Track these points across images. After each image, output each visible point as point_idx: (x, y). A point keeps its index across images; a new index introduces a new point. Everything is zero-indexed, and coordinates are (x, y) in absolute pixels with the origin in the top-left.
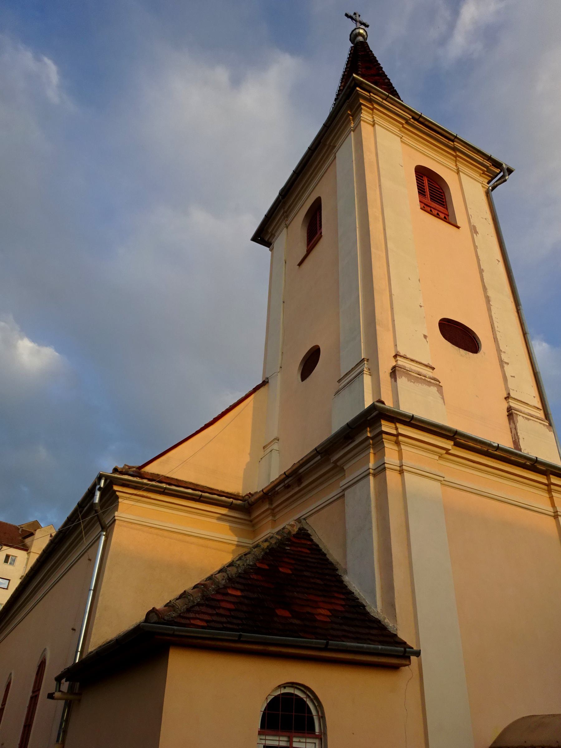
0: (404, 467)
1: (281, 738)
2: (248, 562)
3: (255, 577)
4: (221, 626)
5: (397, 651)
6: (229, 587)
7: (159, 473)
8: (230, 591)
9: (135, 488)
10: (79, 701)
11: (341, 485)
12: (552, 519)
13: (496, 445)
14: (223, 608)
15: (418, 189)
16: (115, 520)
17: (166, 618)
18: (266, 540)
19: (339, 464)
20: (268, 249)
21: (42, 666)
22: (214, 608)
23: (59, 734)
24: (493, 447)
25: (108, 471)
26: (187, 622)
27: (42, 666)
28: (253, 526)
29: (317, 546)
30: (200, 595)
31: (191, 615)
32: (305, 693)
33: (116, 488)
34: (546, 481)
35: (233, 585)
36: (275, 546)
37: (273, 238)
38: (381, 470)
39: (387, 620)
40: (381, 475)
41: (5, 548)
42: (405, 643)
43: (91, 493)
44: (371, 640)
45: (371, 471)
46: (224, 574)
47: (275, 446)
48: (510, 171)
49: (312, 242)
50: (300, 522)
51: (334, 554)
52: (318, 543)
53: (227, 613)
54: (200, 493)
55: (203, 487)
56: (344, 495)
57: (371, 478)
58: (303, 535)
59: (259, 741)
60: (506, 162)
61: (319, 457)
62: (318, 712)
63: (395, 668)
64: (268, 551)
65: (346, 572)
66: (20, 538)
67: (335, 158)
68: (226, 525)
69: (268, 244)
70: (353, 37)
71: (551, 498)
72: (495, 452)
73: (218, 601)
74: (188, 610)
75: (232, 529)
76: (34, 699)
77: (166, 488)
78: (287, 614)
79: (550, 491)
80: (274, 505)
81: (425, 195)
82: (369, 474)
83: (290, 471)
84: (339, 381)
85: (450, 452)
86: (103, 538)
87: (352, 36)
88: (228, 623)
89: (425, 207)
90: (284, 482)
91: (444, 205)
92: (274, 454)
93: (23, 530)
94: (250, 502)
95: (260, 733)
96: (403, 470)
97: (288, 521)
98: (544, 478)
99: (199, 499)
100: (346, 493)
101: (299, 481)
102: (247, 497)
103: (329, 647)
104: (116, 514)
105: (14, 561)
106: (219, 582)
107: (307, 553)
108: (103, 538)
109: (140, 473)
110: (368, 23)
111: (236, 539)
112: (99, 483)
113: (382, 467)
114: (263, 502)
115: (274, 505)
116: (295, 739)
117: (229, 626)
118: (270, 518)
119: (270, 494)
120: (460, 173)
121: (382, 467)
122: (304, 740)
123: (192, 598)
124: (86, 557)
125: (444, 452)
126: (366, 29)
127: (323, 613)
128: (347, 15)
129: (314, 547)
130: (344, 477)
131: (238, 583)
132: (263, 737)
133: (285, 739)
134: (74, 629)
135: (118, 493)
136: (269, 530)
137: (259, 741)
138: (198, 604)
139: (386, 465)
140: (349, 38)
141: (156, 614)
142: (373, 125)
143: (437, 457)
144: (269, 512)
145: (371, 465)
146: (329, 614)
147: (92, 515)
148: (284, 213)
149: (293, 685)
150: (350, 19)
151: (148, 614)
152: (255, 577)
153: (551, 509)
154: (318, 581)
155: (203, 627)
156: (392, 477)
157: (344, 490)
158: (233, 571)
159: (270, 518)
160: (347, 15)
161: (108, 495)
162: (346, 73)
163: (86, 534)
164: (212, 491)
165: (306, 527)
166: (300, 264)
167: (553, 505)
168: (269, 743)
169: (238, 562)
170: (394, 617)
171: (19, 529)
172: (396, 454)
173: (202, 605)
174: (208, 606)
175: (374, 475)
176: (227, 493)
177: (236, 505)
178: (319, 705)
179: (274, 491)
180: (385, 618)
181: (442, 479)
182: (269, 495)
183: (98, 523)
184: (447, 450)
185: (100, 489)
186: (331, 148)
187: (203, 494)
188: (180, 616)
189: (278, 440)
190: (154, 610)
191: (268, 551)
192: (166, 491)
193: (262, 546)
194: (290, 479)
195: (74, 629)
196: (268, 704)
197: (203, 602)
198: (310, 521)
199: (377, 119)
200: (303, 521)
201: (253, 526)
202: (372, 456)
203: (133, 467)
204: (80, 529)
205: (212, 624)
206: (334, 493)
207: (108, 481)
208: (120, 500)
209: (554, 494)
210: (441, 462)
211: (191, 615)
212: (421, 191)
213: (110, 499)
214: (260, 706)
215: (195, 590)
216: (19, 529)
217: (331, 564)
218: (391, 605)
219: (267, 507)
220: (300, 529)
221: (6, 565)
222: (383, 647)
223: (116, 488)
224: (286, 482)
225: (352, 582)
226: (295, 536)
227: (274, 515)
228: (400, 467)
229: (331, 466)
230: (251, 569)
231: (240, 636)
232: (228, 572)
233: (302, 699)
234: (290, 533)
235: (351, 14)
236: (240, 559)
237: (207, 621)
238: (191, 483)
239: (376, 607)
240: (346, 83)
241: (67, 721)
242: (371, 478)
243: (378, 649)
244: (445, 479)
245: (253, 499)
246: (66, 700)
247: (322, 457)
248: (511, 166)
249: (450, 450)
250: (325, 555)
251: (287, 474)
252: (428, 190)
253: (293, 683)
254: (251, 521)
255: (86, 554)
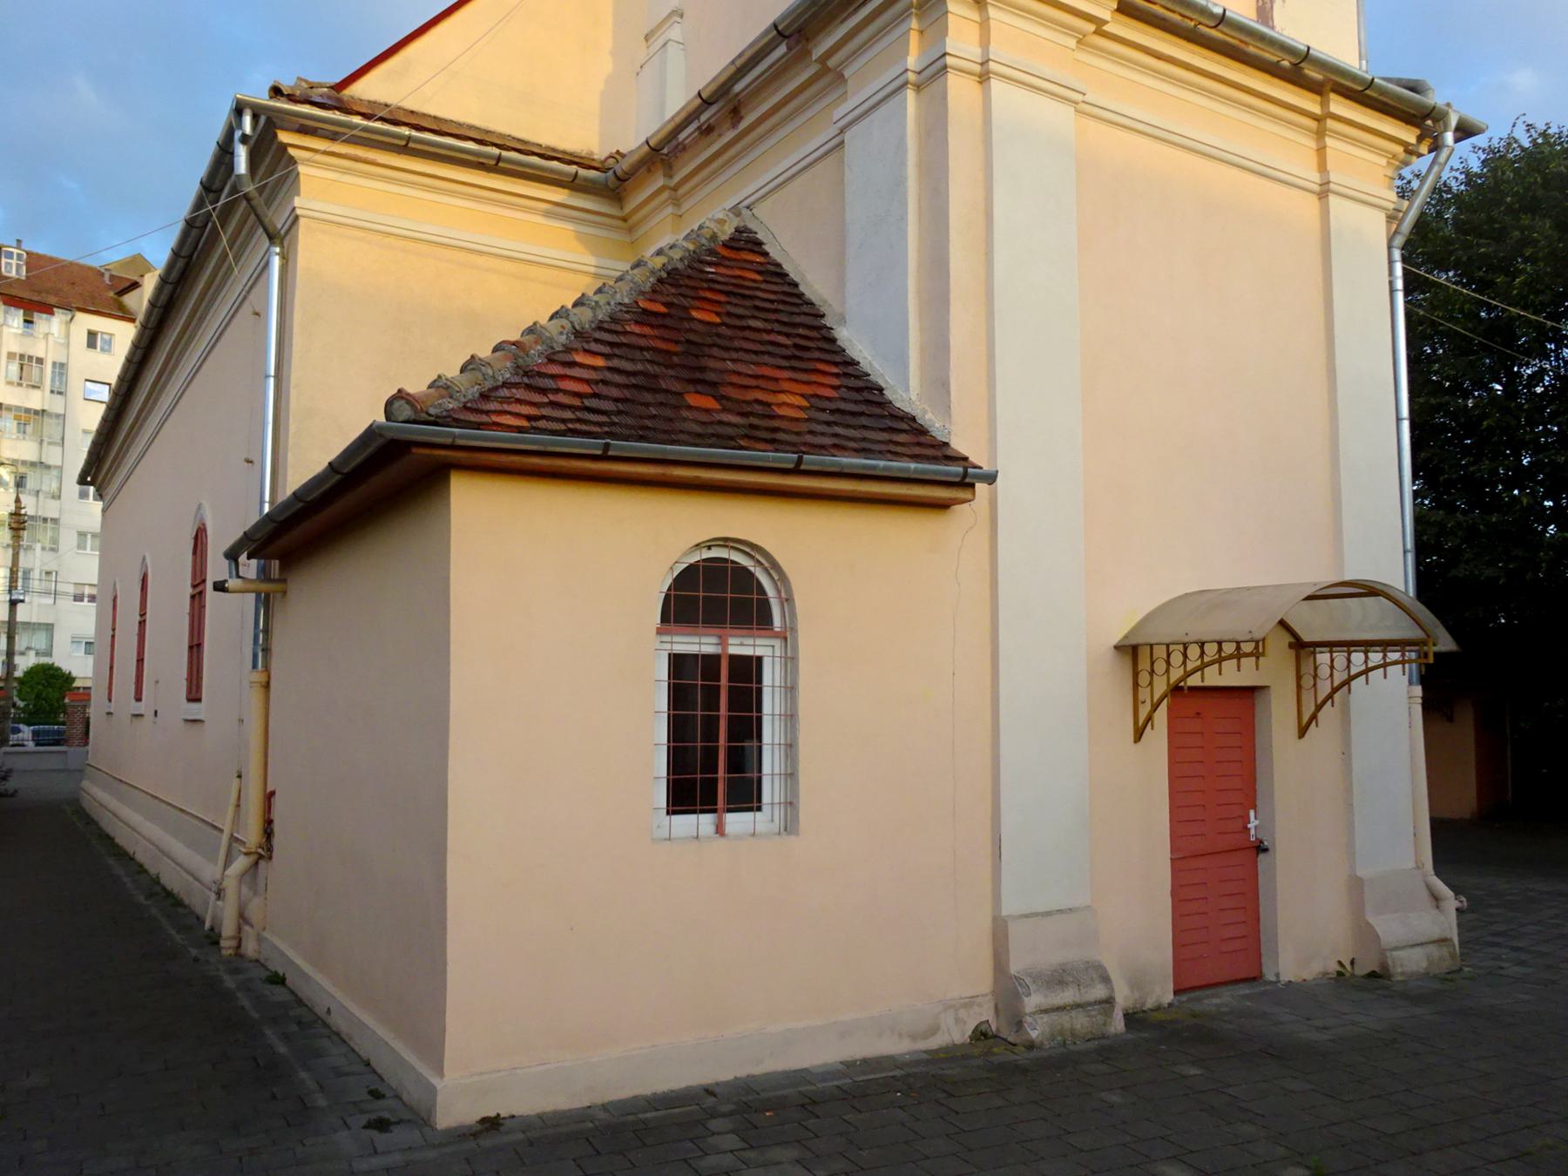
0: (992, 66)
1: (704, 640)
2: (618, 296)
3: (637, 329)
4: (563, 427)
5: (947, 474)
7: (389, 101)
8: (579, 358)
9: (333, 137)
10: (285, 593)
11: (836, 117)
12: (1314, 198)
13: (1218, 10)
14: (566, 392)
16: (297, 218)
17: (432, 411)
18: (660, 253)
19: (831, 63)
21: (200, 537)
22: (543, 391)
23: (255, 656)
24: (1211, 15)
25: (262, 98)
26: (485, 418)
27: (200, 537)
28: (630, 230)
29: (779, 265)
30: (508, 364)
31: (493, 406)
32: (752, 557)
33: (284, 137)
34: (1316, 109)
36: (680, 266)
38: (936, 70)
39: (929, 416)
40: (935, 86)
41: (80, 316)
42: (966, 459)
43: (225, 151)
44: (895, 454)
45: (911, 77)
46: (564, 322)
47: (675, 32)
50: (738, 214)
51: (814, 283)
52: (779, 260)
53: (576, 402)
54: (496, 151)
55: (501, 136)
57: (910, 94)
58: (745, 243)
59: (658, 646)
61: (782, 49)
62: (779, 592)
63: (943, 506)
64: (664, 275)
65: (842, 320)
66: (111, 294)
68: (564, 229)
71: (1321, 151)
72: (1213, 33)
73: (553, 377)
74: (484, 396)
75: (580, 237)
76: (197, 598)
77: (409, 138)
78: (710, 403)
79: (1320, 134)
80: (677, 179)
82: (906, 83)
83: (713, 87)
85: (1105, 28)
86: (276, 262)
88: (579, 420)
90: (698, 118)
92: (671, 48)
93: (112, 277)
94: (619, 173)
95: (659, 632)
96: (988, 72)
97: (711, 211)
98: (1314, 101)
99: (494, 167)
100: (847, 136)
101: (735, 113)
102: (611, 161)
103: (803, 467)
104: (297, 201)
105: (109, 343)
106: (551, 339)
107: (754, 281)
108: (276, 262)
109: (340, 100)
111: (591, 260)
112: (240, 125)
113: (939, 64)
114: (649, 171)
115: (677, 179)
116: (731, 641)
117: (578, 426)
119: (665, 151)
121: (939, 64)
122: (750, 641)
123: (490, 372)
124: (247, 309)
125: (1092, 28)
127: (790, 402)
129: (772, 268)
130: (844, 97)
131: (596, 341)
132: (667, 638)
133: (714, 640)
134: (249, 461)
135: (291, 151)
136: (669, 231)
137: (658, 646)
138: (505, 385)
139: (949, 60)
141: (408, 402)
143: (1072, 43)
144: (666, 195)
145: (912, 61)
146: (805, 403)
147: (236, 209)
149: (725, 542)
151: (389, 404)
152: (637, 329)
153: (1316, 177)
154: (781, 339)
155: (520, 430)
156: (959, 89)
157: (842, 131)
158: (584, 317)
159: (669, 210)
161: (268, 160)
163: (237, 258)
164: (525, 148)
165: (752, 226)
167: (1322, 167)
168: (681, 648)
169: (596, 298)
170: (946, 408)
171: (102, 275)
172: (973, 33)
173: (516, 385)
174: (529, 387)
175: (918, 88)
176: (564, 152)
177: (586, 179)
178: (781, 578)
179: (674, 143)
180: (925, 412)
181: (1079, 97)
182: (662, 154)
183: (261, 230)
184: (1099, 22)
185: (245, 139)
187: (505, 154)
188: (465, 408)
190: (401, 395)
191: (664, 275)
192: (411, 145)
193: (650, 265)
194: (713, 109)
195: (249, 461)
196: (675, 580)
197: (517, 379)
198: (762, 211)
200: (745, 212)
201: (630, 230)
202: (914, 38)
203: (321, 86)
204: (220, 251)
205: (542, 424)
206: (821, 137)
207: (263, 119)
208: (301, 169)
209: (1328, 141)
210: (1083, 56)
211: (493, 406)
213: (271, 157)
214: (662, 583)
215: (498, 354)
216: (102, 275)
218: (940, 385)
220: (737, 230)
221: (91, 352)
222: (920, 466)
223: (284, 137)
224: (703, 118)
225: (855, 340)
226: (725, 245)
227: (677, 202)
228: (982, 64)
231: (607, 446)
232: (573, 318)
233: (745, 569)
234: (714, 237)
236: (599, 291)
237: (529, 418)
238: (471, 127)
239: (907, 389)
241: (266, 631)
242: (910, 94)
243: (908, 470)
244: (1087, 98)
245: (625, 165)
246: (258, 595)
247: (789, 49)
249: (1106, 22)
250: (796, 285)
251: (704, 96)
253: (726, 539)
254: (625, 220)
255: (246, 305)
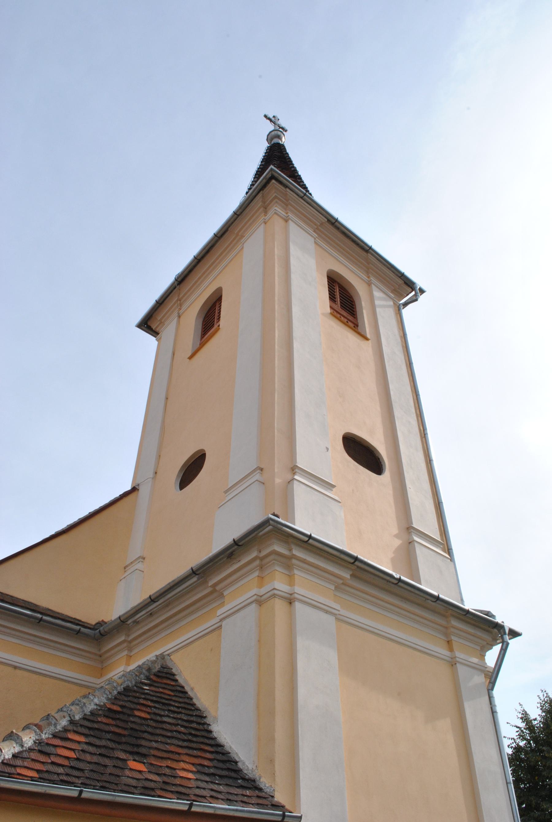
3: (104, 720)
6: (69, 731)
8: (70, 736)
15: (329, 294)
19: (218, 588)
20: (154, 338)
22: (48, 754)
35: (75, 729)
37: (163, 326)
42: (283, 807)
48: (422, 291)
49: (206, 337)
56: (221, 626)
58: (162, 677)
60: (419, 282)
61: (195, 579)
65: (216, 719)
67: (243, 248)
69: (154, 333)
70: (270, 137)
73: (55, 746)
81: (335, 301)
84: (226, 492)
87: (269, 137)
89: (334, 313)
91: (354, 314)
97: (146, 656)
100: (224, 623)
110: (287, 128)
118: (126, 653)
120: (373, 285)
126: (284, 133)
128: (265, 116)
129: (179, 688)
130: (222, 605)
131: (81, 726)
136: (123, 667)
140: (266, 138)
142: (286, 221)
148: (177, 300)
150: (268, 121)
152: (104, 720)
155: (32, 778)
157: (221, 620)
160: (265, 116)
162: (260, 170)
165: (170, 664)
166: (190, 358)
174: (40, 752)
186: (238, 237)
189: (144, 559)
199: (290, 215)
205: (46, 776)
212: (332, 298)
217: (198, 709)
219: (123, 638)
229: (209, 590)
230: (99, 710)
235: (271, 117)
237: (38, 771)
240: (258, 179)
247: (198, 579)
248: (424, 288)
252: (338, 296)
